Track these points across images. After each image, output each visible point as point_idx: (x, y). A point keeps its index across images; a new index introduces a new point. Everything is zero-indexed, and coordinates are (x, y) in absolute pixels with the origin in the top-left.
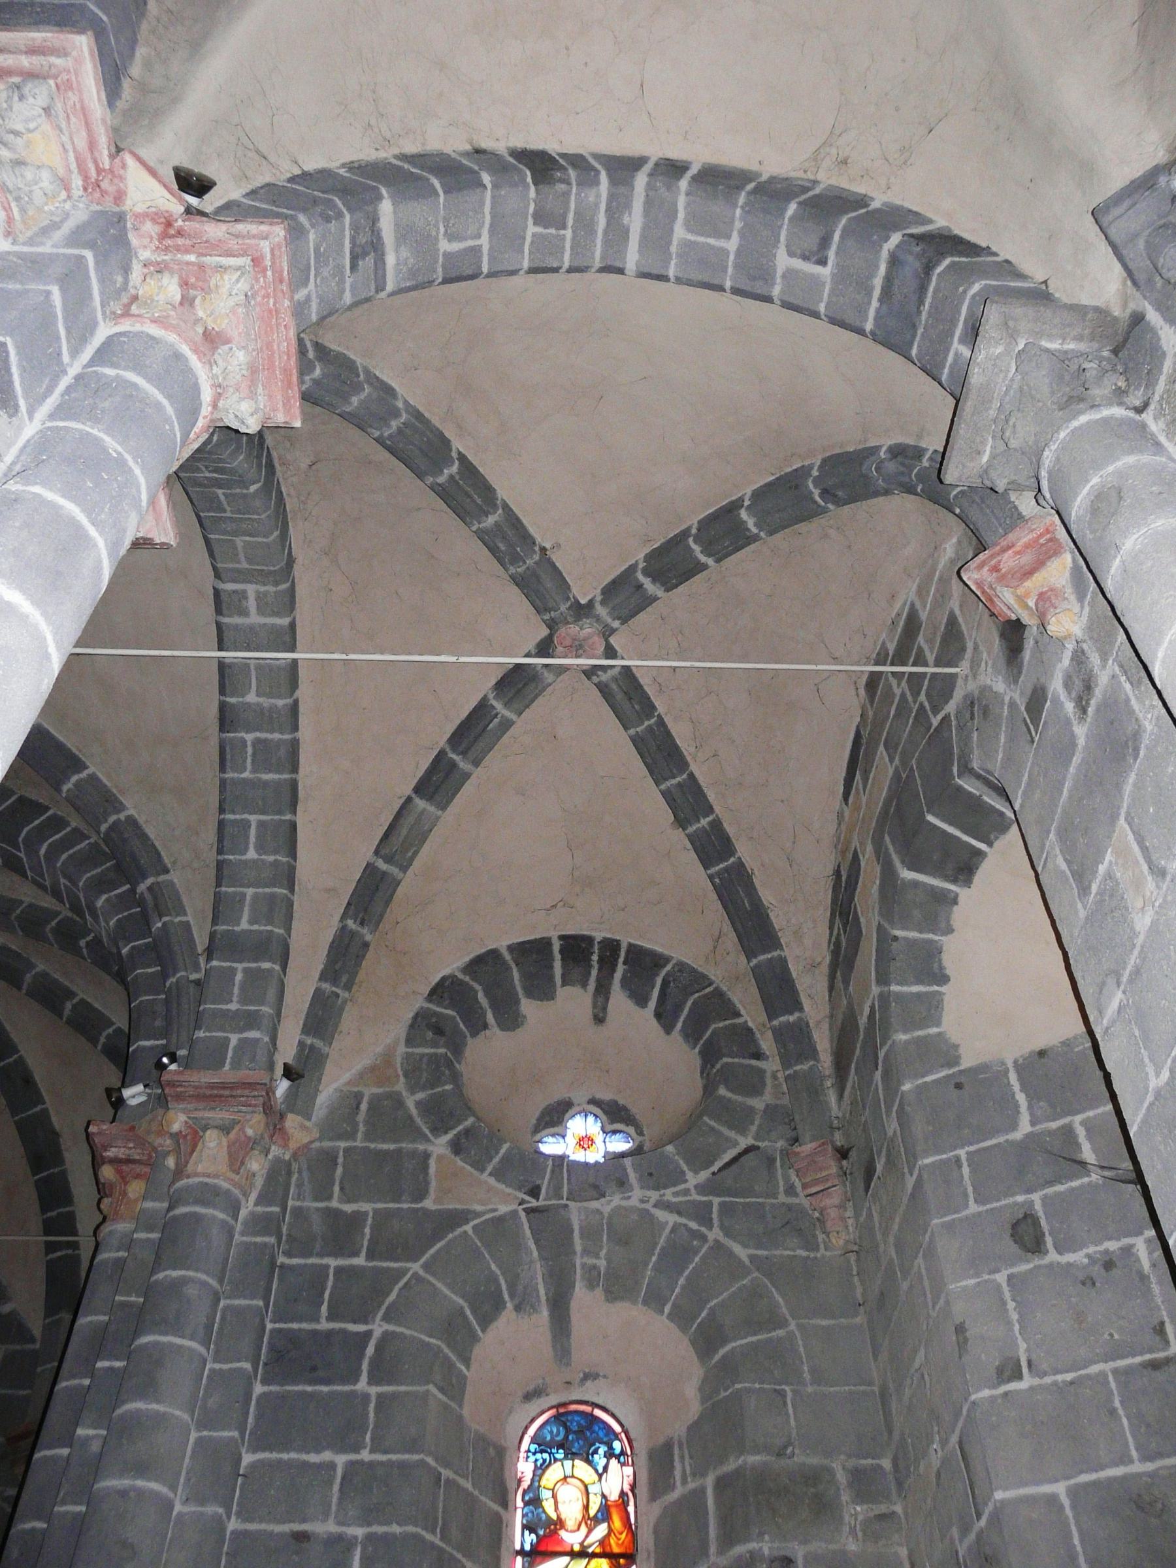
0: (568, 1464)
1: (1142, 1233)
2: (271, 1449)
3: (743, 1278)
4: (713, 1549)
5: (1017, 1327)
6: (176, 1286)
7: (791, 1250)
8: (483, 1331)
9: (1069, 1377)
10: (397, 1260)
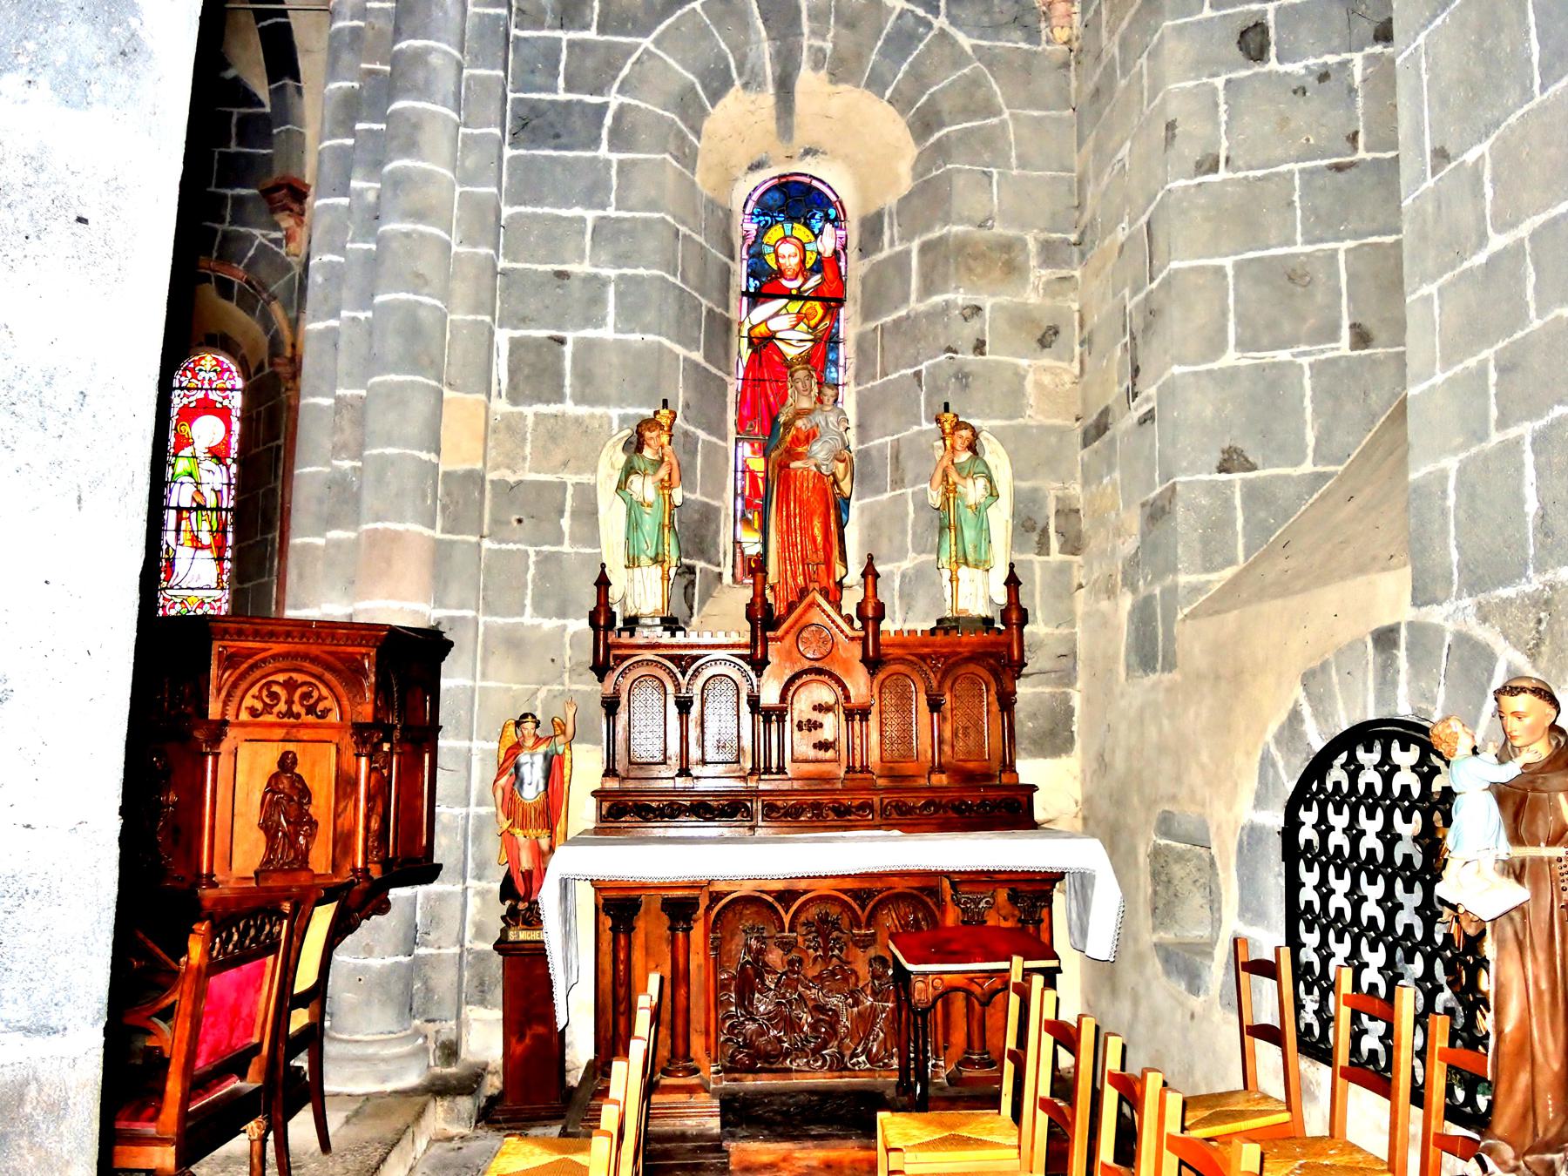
0: (788, 226)
1: (1362, 49)
2: (524, 203)
3: (965, 66)
4: (913, 297)
5: (1223, 128)
6: (420, 57)
7: (1014, 42)
8: (713, 106)
9: (1259, 173)
10: (628, 34)
